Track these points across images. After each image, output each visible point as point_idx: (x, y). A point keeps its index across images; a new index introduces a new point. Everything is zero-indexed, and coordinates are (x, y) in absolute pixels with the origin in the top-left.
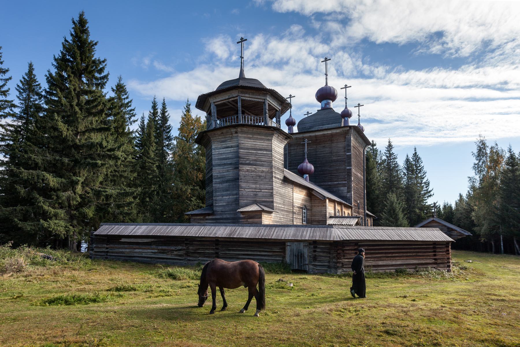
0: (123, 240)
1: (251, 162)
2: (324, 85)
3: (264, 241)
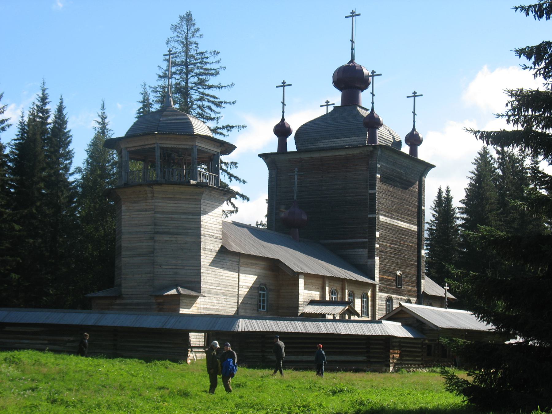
0: (7, 329)
1: (171, 230)
2: (345, 61)
3: (436, 329)
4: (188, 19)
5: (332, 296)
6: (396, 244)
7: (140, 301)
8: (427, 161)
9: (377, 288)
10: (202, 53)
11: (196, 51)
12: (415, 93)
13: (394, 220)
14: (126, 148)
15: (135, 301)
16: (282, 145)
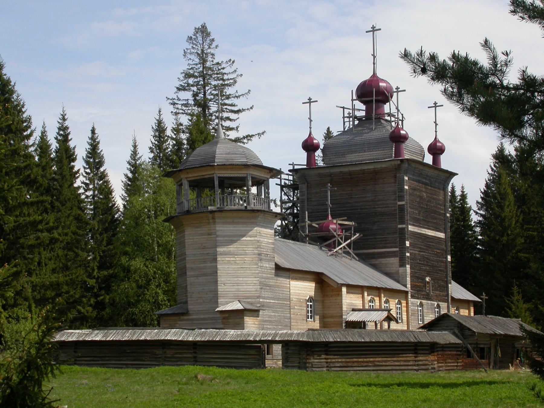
2: (367, 76)
4: (203, 31)
5: (370, 304)
6: (424, 252)
7: (206, 316)
8: (450, 170)
9: (409, 295)
10: (218, 63)
11: (212, 61)
12: (435, 103)
13: (422, 229)
14: (186, 178)
15: (202, 316)
16: (310, 159)
